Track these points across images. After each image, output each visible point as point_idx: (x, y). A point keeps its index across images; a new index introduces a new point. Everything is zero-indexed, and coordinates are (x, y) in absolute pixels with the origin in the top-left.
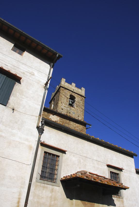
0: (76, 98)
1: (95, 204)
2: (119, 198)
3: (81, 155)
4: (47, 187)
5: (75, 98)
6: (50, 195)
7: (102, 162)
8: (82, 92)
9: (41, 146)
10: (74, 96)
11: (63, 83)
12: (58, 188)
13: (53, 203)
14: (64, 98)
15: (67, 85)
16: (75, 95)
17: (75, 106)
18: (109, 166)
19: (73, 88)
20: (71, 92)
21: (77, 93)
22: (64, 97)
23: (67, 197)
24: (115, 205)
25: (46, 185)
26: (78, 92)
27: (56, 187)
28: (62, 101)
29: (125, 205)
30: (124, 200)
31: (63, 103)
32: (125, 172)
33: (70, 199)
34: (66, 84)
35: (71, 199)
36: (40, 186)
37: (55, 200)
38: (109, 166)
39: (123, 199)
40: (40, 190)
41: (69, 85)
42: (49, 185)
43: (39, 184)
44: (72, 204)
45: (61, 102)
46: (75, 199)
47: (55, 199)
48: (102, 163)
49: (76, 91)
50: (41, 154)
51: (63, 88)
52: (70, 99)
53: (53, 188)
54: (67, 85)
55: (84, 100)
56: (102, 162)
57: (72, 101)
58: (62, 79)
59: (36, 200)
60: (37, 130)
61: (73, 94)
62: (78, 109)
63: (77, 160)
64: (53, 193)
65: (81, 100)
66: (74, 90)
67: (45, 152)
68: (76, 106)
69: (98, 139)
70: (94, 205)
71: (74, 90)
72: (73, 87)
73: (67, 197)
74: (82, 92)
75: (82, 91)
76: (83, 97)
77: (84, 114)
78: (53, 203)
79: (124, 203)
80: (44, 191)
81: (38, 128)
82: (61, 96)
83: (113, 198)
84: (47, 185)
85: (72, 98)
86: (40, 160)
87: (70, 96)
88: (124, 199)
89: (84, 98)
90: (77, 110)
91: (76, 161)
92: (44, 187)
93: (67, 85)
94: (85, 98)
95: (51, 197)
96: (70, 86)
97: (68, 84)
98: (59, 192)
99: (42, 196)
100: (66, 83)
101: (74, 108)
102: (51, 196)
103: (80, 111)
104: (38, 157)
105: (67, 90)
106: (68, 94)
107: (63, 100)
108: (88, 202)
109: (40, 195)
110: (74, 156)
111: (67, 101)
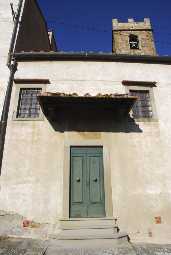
0: (139, 36)
1: (102, 133)
2: (149, 121)
3: (74, 79)
4: (26, 124)
5: (137, 37)
6: (32, 131)
7: (112, 81)
8: (147, 24)
9: (15, 83)
10: (135, 34)
11: (115, 24)
12: (41, 122)
13: (36, 138)
14: (122, 43)
15: (121, 25)
16: (136, 33)
17: (141, 47)
18: (125, 83)
19: (130, 25)
20: (129, 31)
21: (139, 29)
22: (121, 42)
23: (56, 130)
24: (141, 131)
25: (25, 122)
26: (140, 27)
27: (38, 122)
28: (120, 47)
29: (161, 129)
30: (159, 124)
31: (122, 50)
32: (161, 87)
33: (60, 132)
34: (120, 24)
35: (62, 131)
36: (18, 124)
37: (38, 136)
38: (125, 83)
39: (157, 121)
40: (18, 128)
41: (124, 23)
42: (29, 122)
43: (16, 122)
44: (64, 137)
45: (119, 50)
46: (67, 131)
47: (39, 134)
48: (112, 82)
49: (136, 27)
50: (16, 92)
51: (117, 32)
52: (130, 41)
53: (35, 123)
54: (121, 25)
55: (151, 35)
56: (112, 81)
57: (135, 44)
58: (116, 19)
59: (14, 138)
60: (8, 67)
61: (134, 33)
62: (144, 49)
63: (68, 87)
64: (36, 129)
65: (147, 36)
66: (132, 28)
67: (22, 89)
68: (142, 46)
69: (101, 53)
70: (100, 134)
71: (132, 28)
72: (131, 24)
73: (55, 130)
74: (147, 24)
75: (145, 23)
76: (149, 30)
77: (156, 52)
78: (36, 138)
79: (160, 126)
80: (24, 128)
81: (9, 66)
82: (116, 42)
83: (137, 123)
84: (27, 122)
85: (133, 38)
86: (15, 98)
87: (129, 38)
88: (161, 122)
89: (150, 32)
90: (144, 50)
91: (66, 88)
92: (23, 124)
93: (121, 25)
94: (152, 30)
95: (33, 133)
96: (127, 25)
97: (123, 23)
98: (43, 126)
99: (22, 133)
100: (119, 23)
101: (139, 51)
102: (33, 131)
103: (148, 51)
104: (13, 96)
105: (124, 32)
106: (126, 35)
107: (121, 46)
108: (89, 132)
109: (19, 133)
110: (62, 83)
111: (127, 45)
